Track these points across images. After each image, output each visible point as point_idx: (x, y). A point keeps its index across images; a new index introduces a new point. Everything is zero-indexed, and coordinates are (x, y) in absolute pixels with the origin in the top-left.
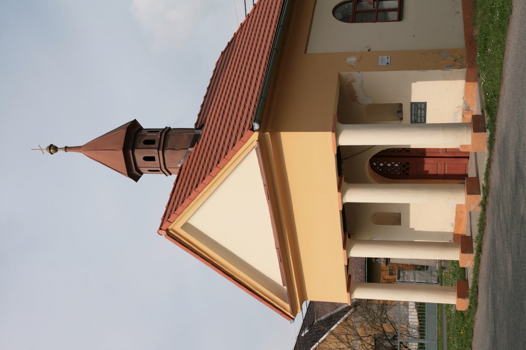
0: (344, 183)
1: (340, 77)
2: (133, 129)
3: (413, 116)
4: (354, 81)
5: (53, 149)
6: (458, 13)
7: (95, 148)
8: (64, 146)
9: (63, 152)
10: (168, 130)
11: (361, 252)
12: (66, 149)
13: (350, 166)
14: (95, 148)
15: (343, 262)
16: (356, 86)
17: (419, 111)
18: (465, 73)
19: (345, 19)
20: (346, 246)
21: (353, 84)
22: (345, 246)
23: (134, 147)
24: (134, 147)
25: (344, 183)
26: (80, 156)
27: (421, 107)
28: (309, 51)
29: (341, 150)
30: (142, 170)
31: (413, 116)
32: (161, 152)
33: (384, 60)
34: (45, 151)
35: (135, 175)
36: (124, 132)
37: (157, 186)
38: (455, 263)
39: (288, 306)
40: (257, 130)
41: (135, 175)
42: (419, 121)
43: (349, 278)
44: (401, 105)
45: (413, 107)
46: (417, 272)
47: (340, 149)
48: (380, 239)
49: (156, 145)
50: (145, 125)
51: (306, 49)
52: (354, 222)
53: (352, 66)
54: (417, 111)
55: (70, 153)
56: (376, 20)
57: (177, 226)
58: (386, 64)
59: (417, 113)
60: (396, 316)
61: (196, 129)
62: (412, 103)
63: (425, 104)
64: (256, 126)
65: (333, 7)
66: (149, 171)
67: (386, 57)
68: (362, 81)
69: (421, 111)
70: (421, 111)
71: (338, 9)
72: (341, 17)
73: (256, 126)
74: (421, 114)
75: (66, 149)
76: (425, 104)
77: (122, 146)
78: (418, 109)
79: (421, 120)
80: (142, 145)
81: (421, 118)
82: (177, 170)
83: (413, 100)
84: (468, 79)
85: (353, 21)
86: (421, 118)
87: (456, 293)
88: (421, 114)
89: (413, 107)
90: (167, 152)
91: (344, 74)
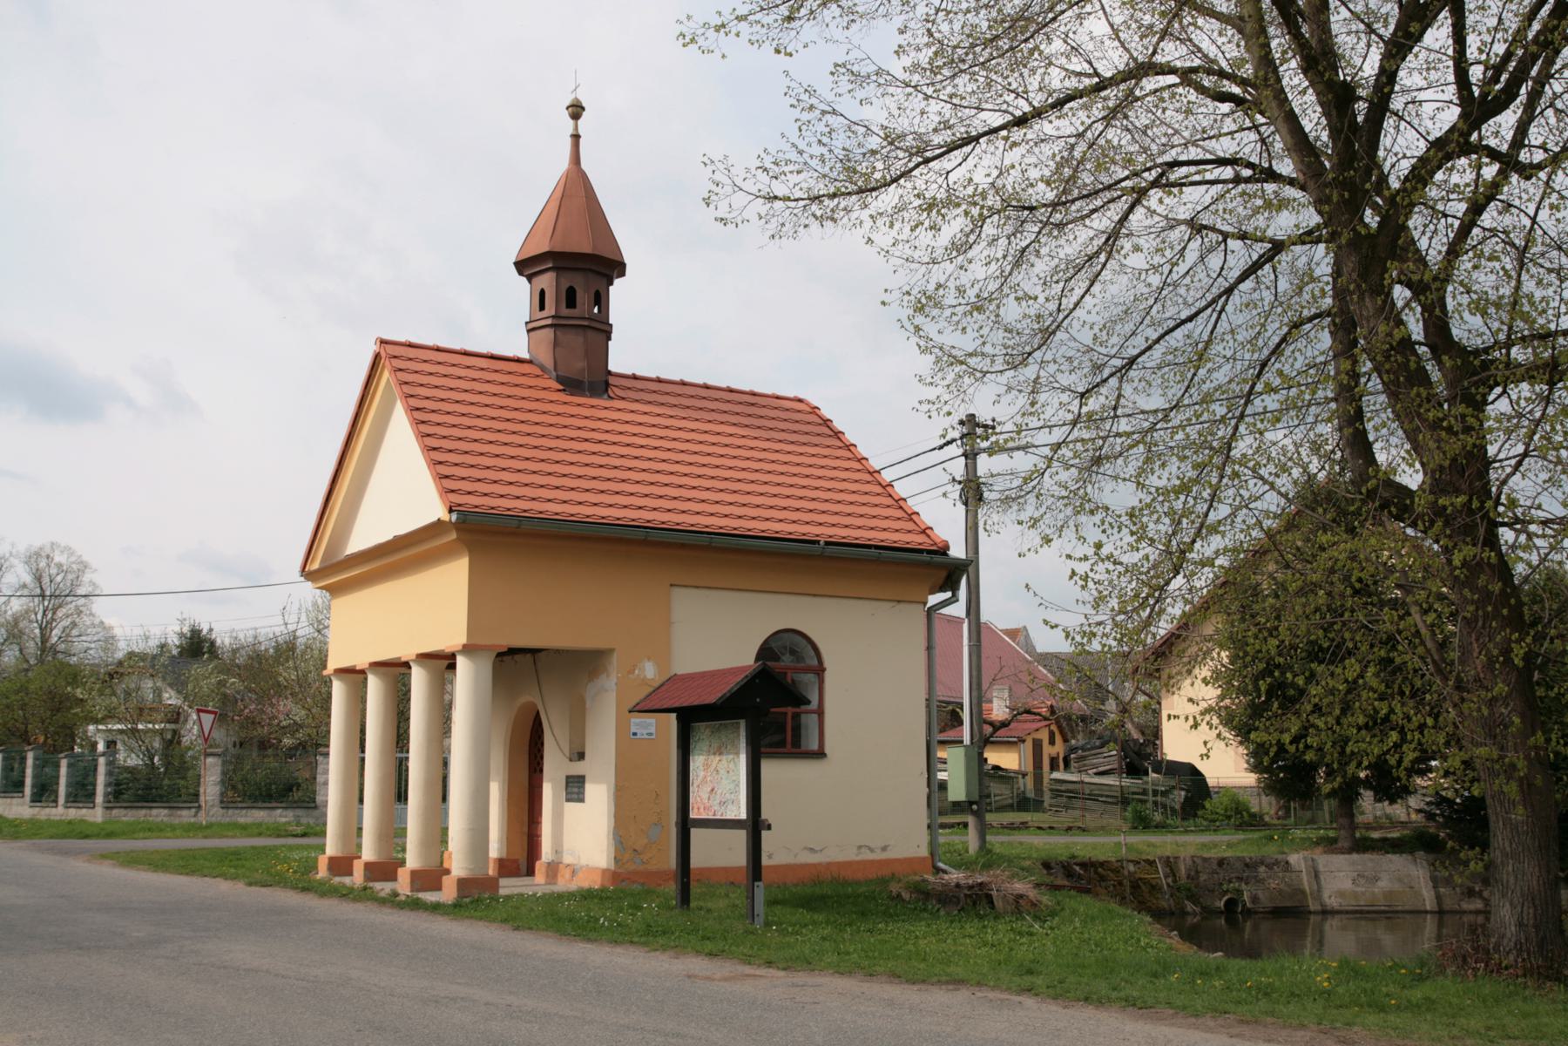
1: (611, 651)
2: (610, 267)
5: (576, 111)
7: (577, 194)
8: (581, 132)
9: (571, 131)
10: (607, 332)
12: (576, 137)
14: (577, 194)
20: (425, 657)
23: (576, 270)
24: (576, 270)
26: (563, 163)
28: (677, 592)
32: (549, 322)
38: (403, 863)
41: (524, 266)
47: (453, 656)
49: (565, 312)
50: (618, 291)
53: (631, 672)
55: (568, 142)
58: (633, 730)
63: (582, 800)
66: (542, 293)
67: (653, 730)
75: (576, 137)
76: (582, 800)
77: (558, 249)
80: (565, 285)
84: (604, 871)
87: (504, 856)
90: (549, 333)
91: (615, 658)
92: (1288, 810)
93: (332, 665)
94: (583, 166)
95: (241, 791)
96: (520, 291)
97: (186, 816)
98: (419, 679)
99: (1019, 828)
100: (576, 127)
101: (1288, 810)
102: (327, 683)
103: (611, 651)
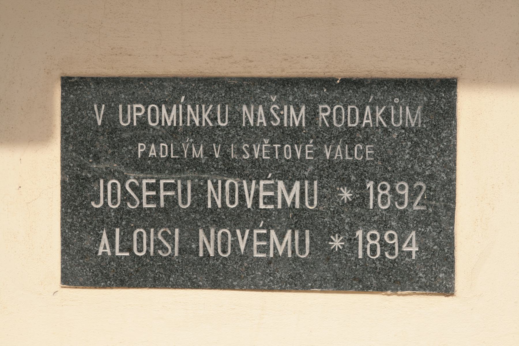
3: (199, 116)
17: (289, 194)
27: (360, 213)
31: (199, 116)
33: (106, 200)
42: (107, 194)
45: (371, 117)
46: (283, 100)
54: (288, 173)
59: (256, 170)
60: (138, 86)
62: (438, 95)
69: (296, 218)
70: (296, 218)
74: (241, 217)
76: (448, 290)
78: (330, 174)
79: (127, 219)
81: (165, 216)
83: (471, 106)
86: (165, 216)
88: (241, 217)
89: (371, 117)
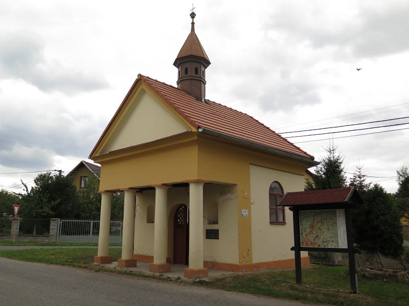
0: (135, 191)
4: (232, 194)
5: (193, 15)
6: (275, 258)
7: (193, 40)
11: (127, 199)
12: (193, 23)
13: (178, 190)
14: (193, 40)
15: (121, 187)
16: (229, 195)
17: (213, 235)
18: (236, 264)
19: (271, 189)
21: (230, 194)
22: (164, 185)
23: (192, 61)
24: (192, 61)
25: (168, 187)
26: (189, 32)
28: (251, 166)
29: (153, 190)
30: (180, 67)
34: (192, 11)
35: (177, 63)
36: (202, 56)
37: (170, 76)
39: (97, 155)
40: (198, 131)
43: (115, 192)
44: (217, 223)
47: (185, 186)
48: (138, 208)
50: (208, 71)
51: (252, 164)
52: (146, 192)
56: (271, 209)
57: (143, 86)
61: (205, 100)
64: (200, 130)
65: (279, 182)
68: (232, 199)
71: (276, 183)
72: (273, 186)
73: (200, 130)
75: (193, 23)
82: (180, 88)
85: (270, 195)
92: (405, 170)
93: (102, 188)
94: (196, 32)
95: (25, 230)
96: (175, 71)
97: (46, 240)
98: (196, 197)
99: (128, 274)
100: (193, 21)
101: (405, 170)
102: (100, 195)
103: (236, 185)
